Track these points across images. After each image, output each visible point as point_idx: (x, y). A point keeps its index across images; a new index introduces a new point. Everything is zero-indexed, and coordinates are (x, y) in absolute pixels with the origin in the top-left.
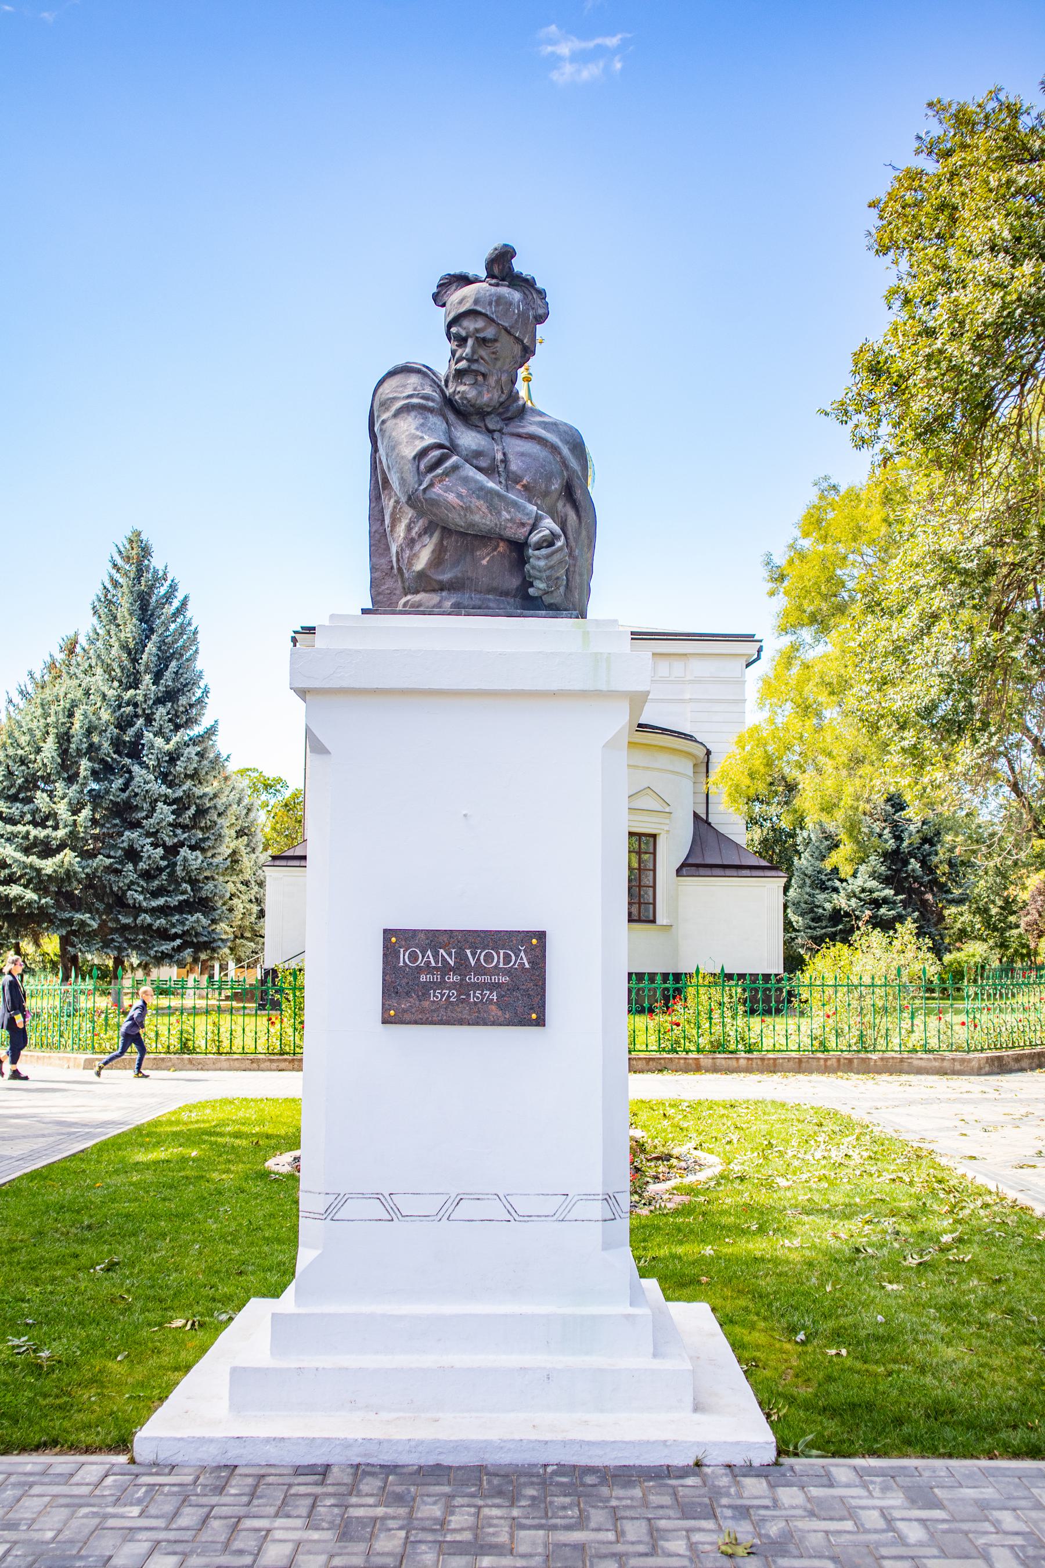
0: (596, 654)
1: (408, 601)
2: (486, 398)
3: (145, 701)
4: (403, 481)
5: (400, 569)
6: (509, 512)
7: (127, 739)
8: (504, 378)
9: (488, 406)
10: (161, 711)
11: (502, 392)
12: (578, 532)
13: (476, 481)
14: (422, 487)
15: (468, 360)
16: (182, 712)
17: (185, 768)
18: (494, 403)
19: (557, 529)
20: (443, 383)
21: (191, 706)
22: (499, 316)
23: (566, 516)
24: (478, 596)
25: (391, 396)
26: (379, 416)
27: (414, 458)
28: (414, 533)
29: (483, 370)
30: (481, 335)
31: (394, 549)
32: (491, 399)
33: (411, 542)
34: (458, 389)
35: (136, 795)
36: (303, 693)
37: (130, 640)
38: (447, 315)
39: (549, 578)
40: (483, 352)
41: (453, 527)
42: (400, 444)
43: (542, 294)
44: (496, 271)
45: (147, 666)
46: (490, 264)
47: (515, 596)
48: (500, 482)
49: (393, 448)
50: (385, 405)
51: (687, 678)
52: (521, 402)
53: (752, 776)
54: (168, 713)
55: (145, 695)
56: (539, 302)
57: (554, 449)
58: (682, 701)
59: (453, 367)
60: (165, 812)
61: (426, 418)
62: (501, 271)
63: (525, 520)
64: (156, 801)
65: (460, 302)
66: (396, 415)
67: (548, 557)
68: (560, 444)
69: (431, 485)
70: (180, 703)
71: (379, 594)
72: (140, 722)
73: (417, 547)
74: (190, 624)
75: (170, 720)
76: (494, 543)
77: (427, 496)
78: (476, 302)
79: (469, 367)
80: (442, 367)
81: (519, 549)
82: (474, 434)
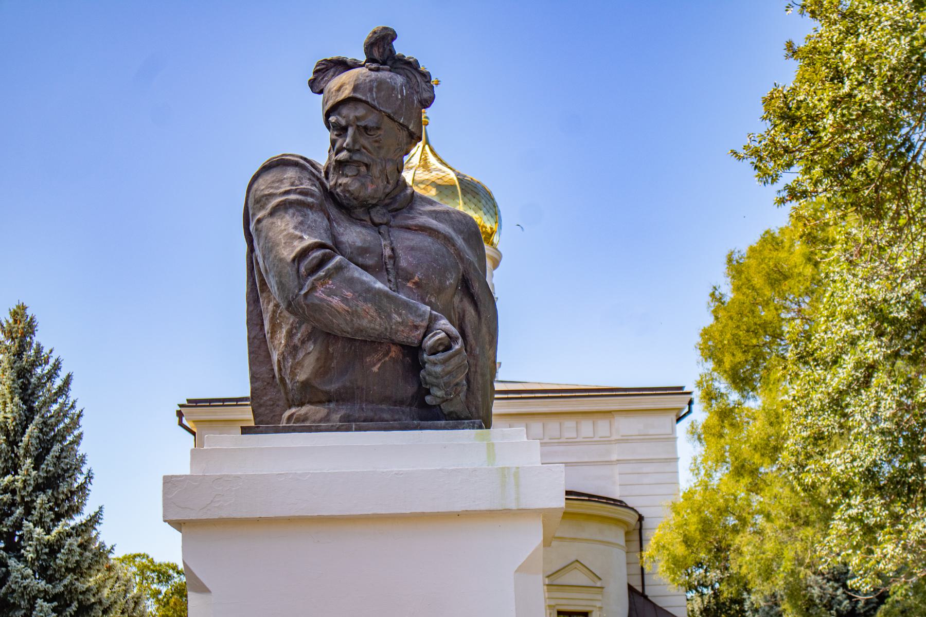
0: (503, 469)
1: (292, 415)
2: (370, 189)
3: (24, 488)
4: (281, 286)
5: (282, 380)
6: (400, 315)
7: (5, 529)
8: (390, 168)
9: (373, 198)
10: (41, 499)
11: (388, 182)
12: (478, 329)
13: (363, 283)
14: (303, 292)
15: (349, 150)
16: (63, 500)
17: (66, 561)
18: (380, 194)
19: (454, 331)
20: (323, 175)
21: (72, 493)
22: (383, 100)
23: (464, 311)
24: (370, 407)
25: (266, 192)
26: (254, 215)
27: (294, 260)
28: (296, 341)
29: (366, 160)
30: (362, 123)
31: (275, 357)
32: (376, 191)
33: (292, 350)
34: (340, 181)
35: (14, 591)
36: (178, 525)
37: (10, 421)
38: (325, 102)
39: (447, 384)
40: (364, 141)
41: (339, 334)
42: (278, 245)
43: (426, 76)
44: (376, 55)
45: (27, 450)
46: (370, 47)
47: (410, 405)
48: (389, 281)
49: (271, 250)
50: (261, 202)
51: (614, 437)
52: (409, 191)
53: (687, 541)
54: (49, 501)
55: (25, 481)
56: (424, 85)
57: (448, 239)
58: (609, 463)
59: (334, 158)
60: (45, 609)
61: (305, 216)
62: (382, 55)
63: (418, 322)
64: (35, 598)
65: (339, 90)
66: (272, 214)
67: (444, 362)
68: (453, 234)
69: (313, 288)
70: (61, 489)
71: (261, 406)
72: (19, 511)
73: (301, 355)
74: (73, 407)
75: (51, 509)
76: (385, 347)
77: (308, 302)
78: (356, 88)
79: (351, 158)
80: (322, 157)
81: (413, 355)
82: (358, 229)
